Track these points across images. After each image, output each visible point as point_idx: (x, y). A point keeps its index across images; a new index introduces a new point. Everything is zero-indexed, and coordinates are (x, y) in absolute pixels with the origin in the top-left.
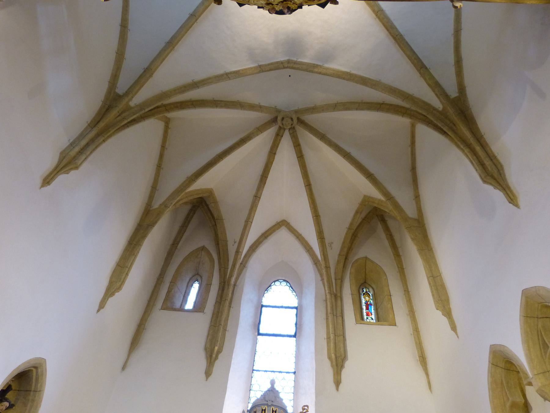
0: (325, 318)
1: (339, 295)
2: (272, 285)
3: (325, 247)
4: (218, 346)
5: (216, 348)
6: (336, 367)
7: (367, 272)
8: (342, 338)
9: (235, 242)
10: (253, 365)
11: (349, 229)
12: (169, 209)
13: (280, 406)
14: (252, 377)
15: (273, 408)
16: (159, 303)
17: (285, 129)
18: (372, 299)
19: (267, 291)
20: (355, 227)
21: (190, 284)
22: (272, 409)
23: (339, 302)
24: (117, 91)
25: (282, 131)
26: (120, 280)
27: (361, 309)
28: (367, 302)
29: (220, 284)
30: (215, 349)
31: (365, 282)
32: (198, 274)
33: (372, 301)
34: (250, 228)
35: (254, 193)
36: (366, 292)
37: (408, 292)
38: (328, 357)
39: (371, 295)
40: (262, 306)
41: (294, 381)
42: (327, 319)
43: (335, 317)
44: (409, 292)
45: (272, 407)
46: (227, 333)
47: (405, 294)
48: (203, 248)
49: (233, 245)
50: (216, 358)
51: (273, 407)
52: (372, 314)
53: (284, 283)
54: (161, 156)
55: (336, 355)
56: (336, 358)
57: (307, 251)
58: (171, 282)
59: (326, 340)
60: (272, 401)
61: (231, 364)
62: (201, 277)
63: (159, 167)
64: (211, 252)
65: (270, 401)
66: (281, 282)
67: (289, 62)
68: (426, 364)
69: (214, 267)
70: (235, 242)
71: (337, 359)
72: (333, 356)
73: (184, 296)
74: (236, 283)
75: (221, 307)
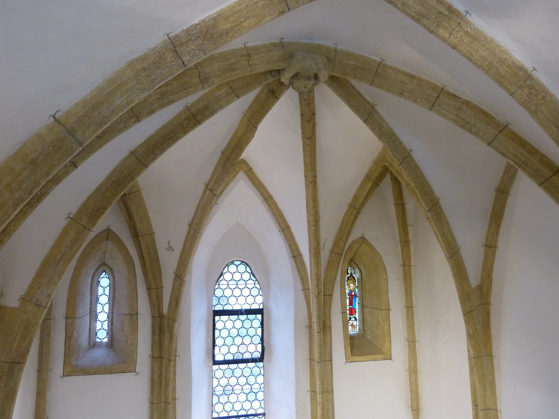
21: (95, 284)
32: (104, 264)
36: (351, 274)
39: (356, 280)
48: (108, 234)
52: (356, 312)
57: (280, 230)
58: (66, 318)
69: (136, 275)
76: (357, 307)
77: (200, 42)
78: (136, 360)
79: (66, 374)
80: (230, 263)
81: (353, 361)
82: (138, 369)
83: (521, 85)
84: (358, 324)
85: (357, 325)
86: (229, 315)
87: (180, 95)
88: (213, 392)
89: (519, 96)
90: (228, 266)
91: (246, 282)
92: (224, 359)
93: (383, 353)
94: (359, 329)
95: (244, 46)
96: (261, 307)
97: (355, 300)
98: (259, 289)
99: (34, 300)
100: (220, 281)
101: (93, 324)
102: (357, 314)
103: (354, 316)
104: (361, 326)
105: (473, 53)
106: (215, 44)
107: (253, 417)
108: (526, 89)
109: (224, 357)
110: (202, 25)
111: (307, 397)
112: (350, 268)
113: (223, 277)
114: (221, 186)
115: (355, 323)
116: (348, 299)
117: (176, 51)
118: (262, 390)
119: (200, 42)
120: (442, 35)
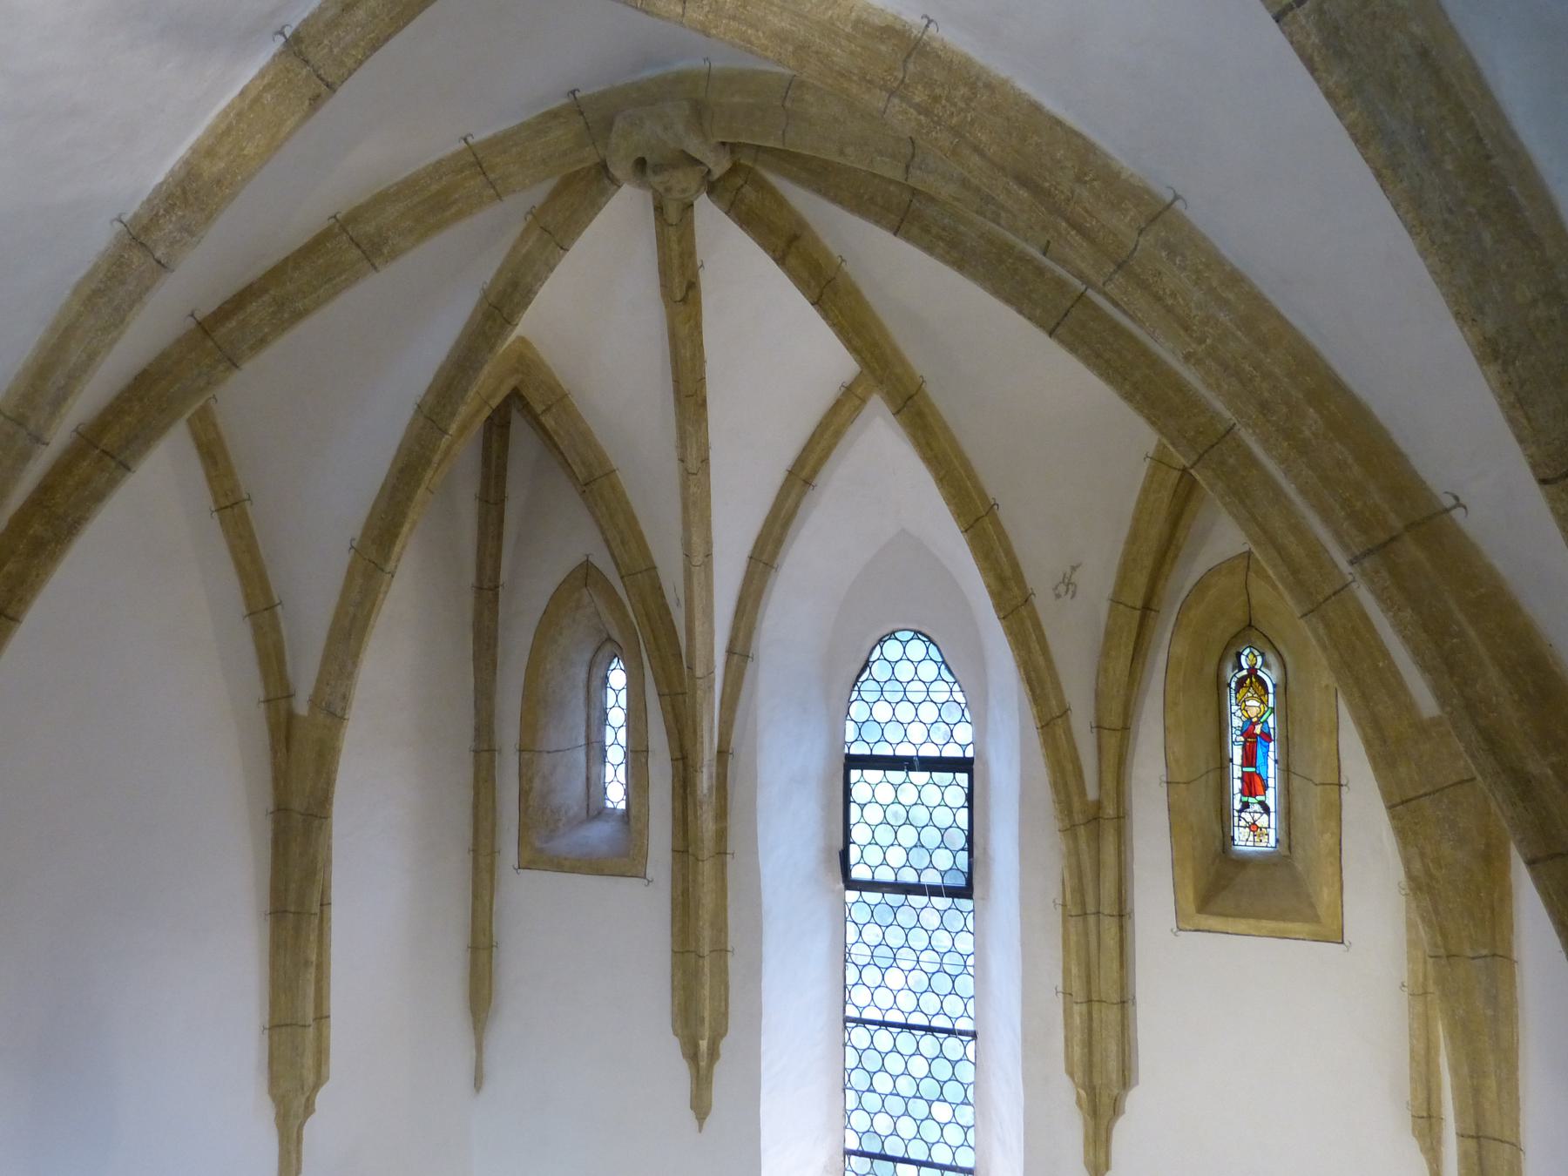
1: (1110, 810)
21: (596, 682)
27: (1224, 763)
28: (1252, 722)
31: (1250, 625)
36: (1252, 671)
39: (1271, 689)
46: (732, 962)
50: (714, 1054)
52: (1266, 787)
58: (520, 751)
76: (1271, 771)
77: (180, 213)
79: (525, 864)
80: (887, 635)
81: (1201, 928)
82: (650, 873)
83: (903, 81)
84: (1273, 825)
85: (1269, 827)
86: (885, 769)
87: (318, 297)
88: (847, 955)
89: (900, 117)
90: (882, 643)
91: (905, 684)
92: (873, 878)
93: (1315, 919)
94: (1277, 841)
95: (465, 145)
96: (970, 753)
97: (1265, 750)
98: (963, 706)
99: (324, 704)
100: (863, 682)
101: (594, 770)
102: (1271, 793)
103: (1259, 798)
104: (1282, 833)
105: (749, 31)
106: (203, 210)
107: (924, 1033)
108: (919, 87)
109: (896, 875)
110: (169, 184)
112: (1246, 652)
113: (870, 673)
115: (1263, 821)
116: (1240, 747)
117: (141, 243)
118: (971, 970)
119: (180, 213)
120: (666, 12)
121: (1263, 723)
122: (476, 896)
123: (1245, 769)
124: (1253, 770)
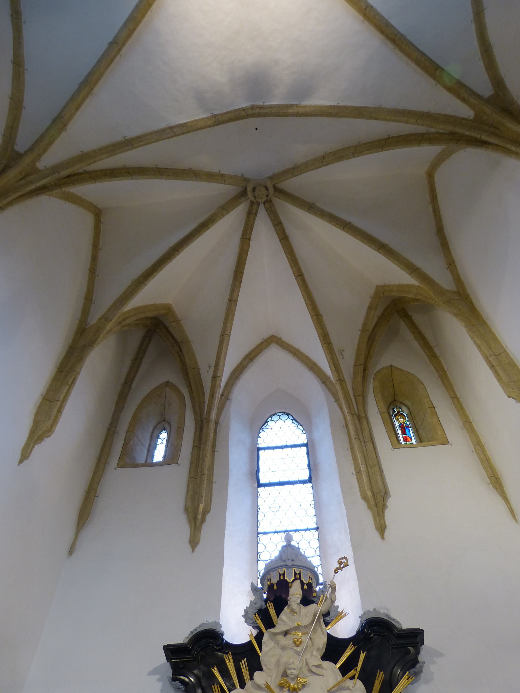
0: (349, 448)
1: (363, 415)
2: (268, 421)
3: (334, 354)
4: (203, 502)
5: (201, 506)
6: (376, 508)
7: (395, 385)
8: (376, 468)
9: (210, 367)
10: (256, 527)
11: (363, 330)
12: (112, 322)
13: (302, 565)
14: (258, 543)
15: (294, 570)
16: (114, 461)
17: (258, 204)
18: (408, 420)
19: (263, 429)
20: (370, 327)
21: (155, 435)
22: (293, 571)
23: (365, 424)
24: (16, 148)
25: (255, 206)
26: (50, 418)
27: (396, 434)
28: (402, 424)
29: (196, 424)
30: (200, 507)
31: (395, 400)
33: (408, 423)
34: (228, 345)
35: (227, 297)
36: (399, 412)
37: (458, 399)
38: (361, 497)
39: (406, 415)
40: (259, 449)
41: (319, 540)
42: (352, 448)
43: (363, 443)
44: (459, 399)
45: (293, 569)
46: (214, 486)
47: (454, 403)
48: (167, 384)
49: (208, 372)
50: (203, 520)
51: (295, 569)
52: (411, 439)
53: (285, 417)
54: (94, 259)
55: (372, 492)
56: (373, 495)
57: (309, 369)
58: (127, 432)
59: (355, 475)
60: (293, 560)
61: (225, 526)
62: (169, 424)
63: (93, 272)
64: (179, 386)
65: (288, 560)
66: (280, 416)
67: (252, 107)
68: (502, 486)
70: (210, 367)
71: (376, 496)
72: (369, 493)
73: (148, 451)
74: (218, 421)
75: (201, 452)
78: (179, 456)
98: (302, 430)
111: (354, 480)
114: (235, 291)
121: (406, 424)
122: (95, 473)
123: (403, 435)
124: (406, 435)
